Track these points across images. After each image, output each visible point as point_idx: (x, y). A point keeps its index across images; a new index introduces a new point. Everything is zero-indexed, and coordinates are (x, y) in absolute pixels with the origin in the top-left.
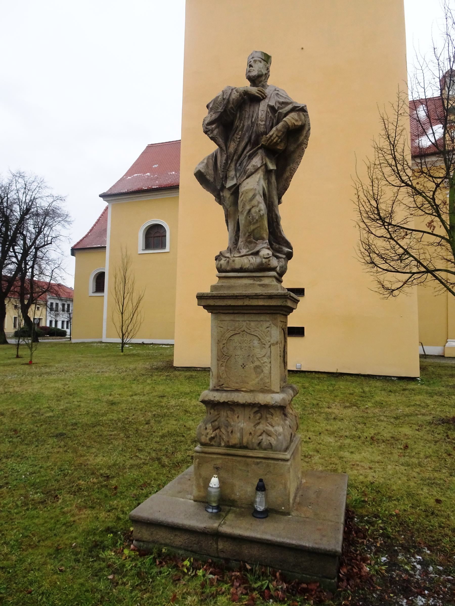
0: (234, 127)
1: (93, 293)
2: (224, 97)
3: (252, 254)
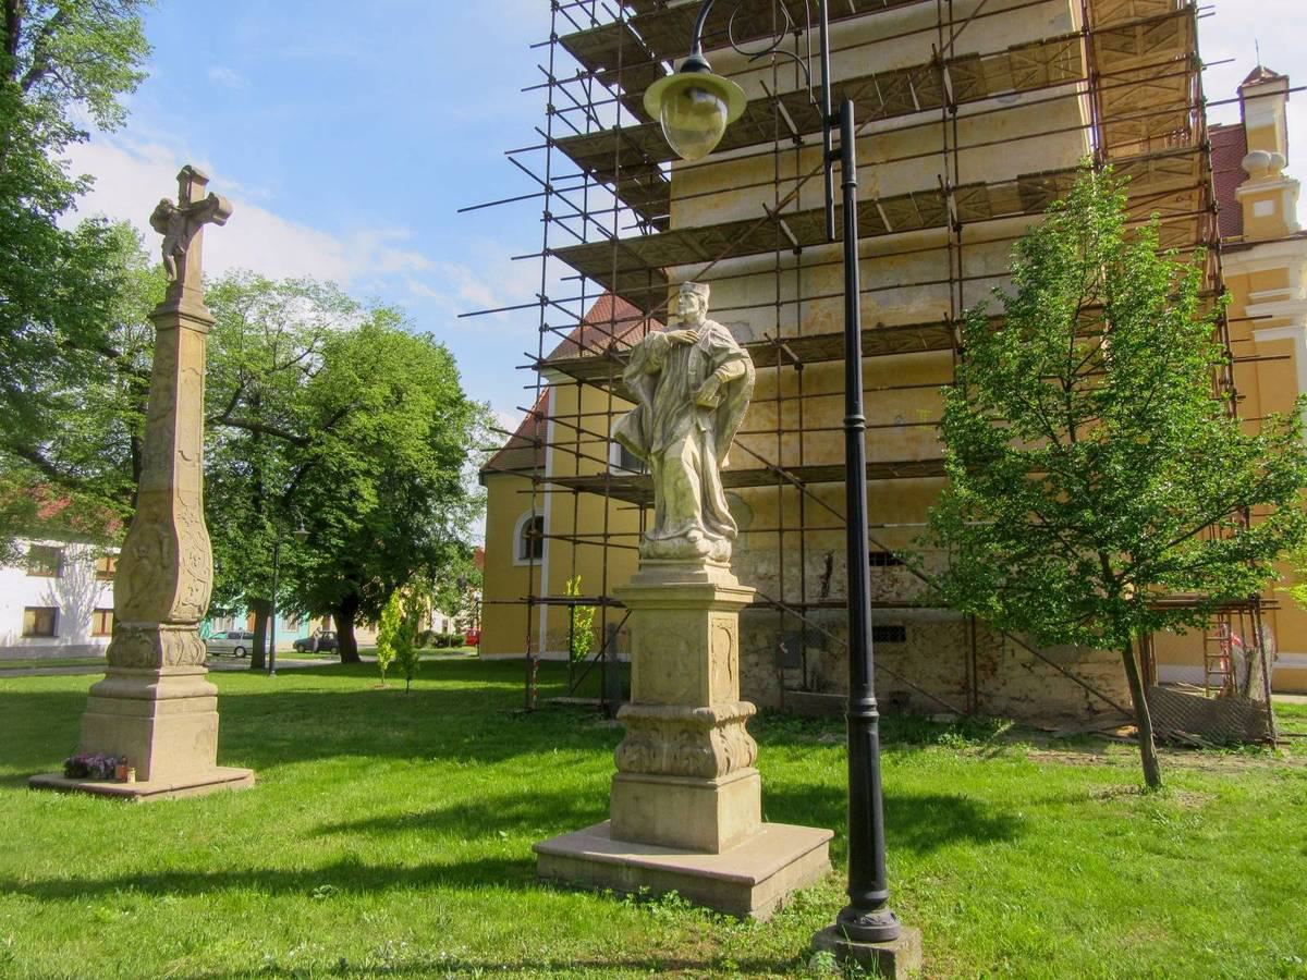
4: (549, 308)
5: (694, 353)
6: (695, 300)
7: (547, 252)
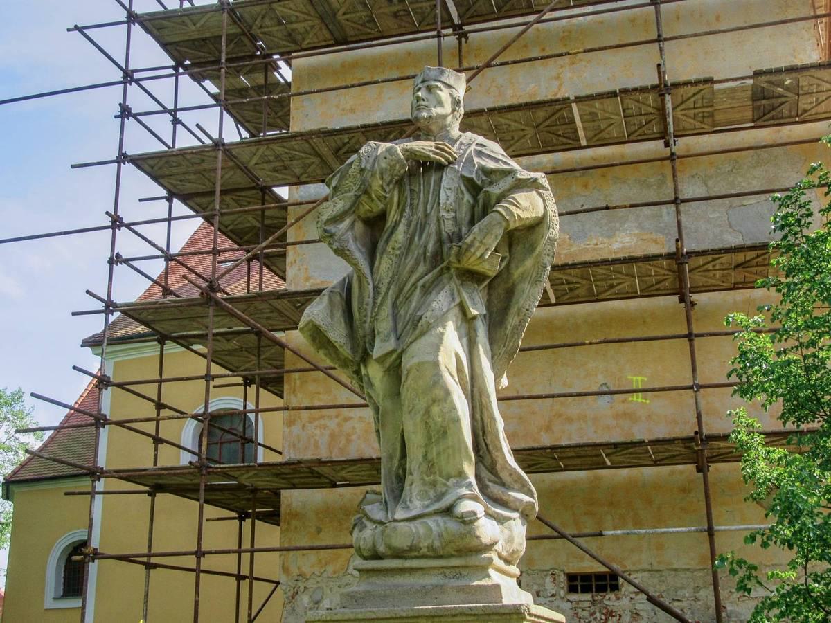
0: (388, 224)
1: (55, 599)
2: (363, 167)
3: (436, 513)
4: (123, 233)
5: (449, 181)
6: (444, 95)
7: (123, 158)
